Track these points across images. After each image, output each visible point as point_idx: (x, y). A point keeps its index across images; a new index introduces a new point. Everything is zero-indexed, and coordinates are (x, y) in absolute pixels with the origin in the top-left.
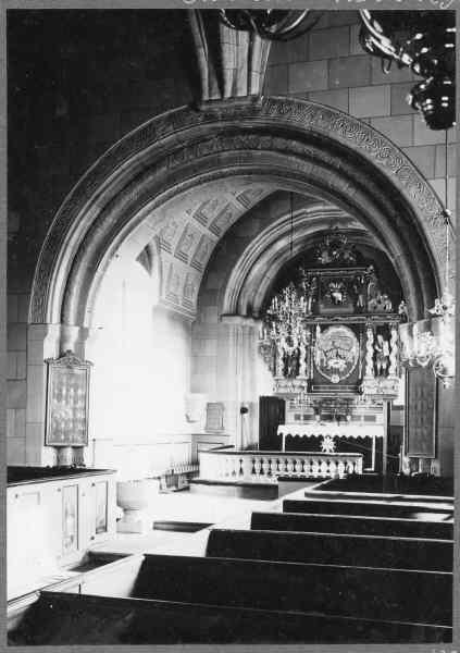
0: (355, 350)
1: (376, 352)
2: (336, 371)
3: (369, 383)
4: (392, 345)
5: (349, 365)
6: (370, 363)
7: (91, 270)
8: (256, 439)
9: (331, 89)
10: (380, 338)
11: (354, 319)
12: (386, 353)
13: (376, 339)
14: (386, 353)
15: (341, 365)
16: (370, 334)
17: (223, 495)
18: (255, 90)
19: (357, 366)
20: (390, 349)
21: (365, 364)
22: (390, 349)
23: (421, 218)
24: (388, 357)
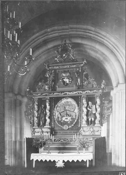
1: (88, 111)
2: (65, 123)
4: (97, 107)
6: (85, 118)
13: (88, 104)
14: (94, 112)
16: (84, 101)
24: (95, 114)
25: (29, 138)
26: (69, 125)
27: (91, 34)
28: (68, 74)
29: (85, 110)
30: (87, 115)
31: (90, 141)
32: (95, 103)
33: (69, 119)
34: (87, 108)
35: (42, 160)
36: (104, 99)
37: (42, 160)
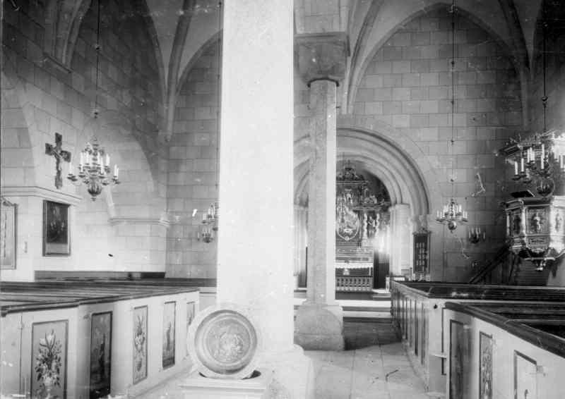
0: (358, 223)
1: (368, 224)
2: (348, 235)
3: (365, 241)
4: (377, 221)
5: (354, 231)
6: (366, 230)
7: (168, 340)
8: (412, 265)
9: (384, 115)
10: (371, 218)
11: (356, 208)
12: (374, 226)
13: (368, 218)
14: (374, 226)
15: (350, 231)
16: (366, 216)
17: (212, 39)
18: (350, 112)
19: (359, 233)
20: (376, 223)
21: (363, 231)
22: (376, 223)
23: (413, 157)
24: (374, 228)
25: (354, 269)
26: (350, 236)
27: (550, 308)
28: (350, 190)
29: (366, 224)
30: (368, 228)
31: (486, 273)
32: (375, 218)
33: (350, 230)
34: (367, 222)
35: (336, 269)
36: (13, 39)
37: (336, 269)
